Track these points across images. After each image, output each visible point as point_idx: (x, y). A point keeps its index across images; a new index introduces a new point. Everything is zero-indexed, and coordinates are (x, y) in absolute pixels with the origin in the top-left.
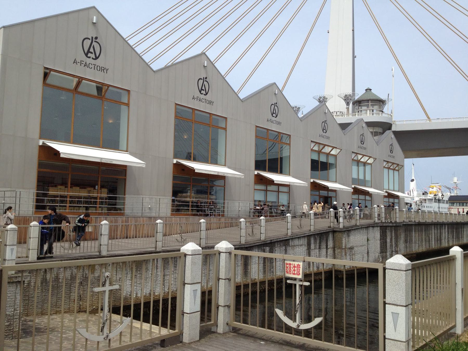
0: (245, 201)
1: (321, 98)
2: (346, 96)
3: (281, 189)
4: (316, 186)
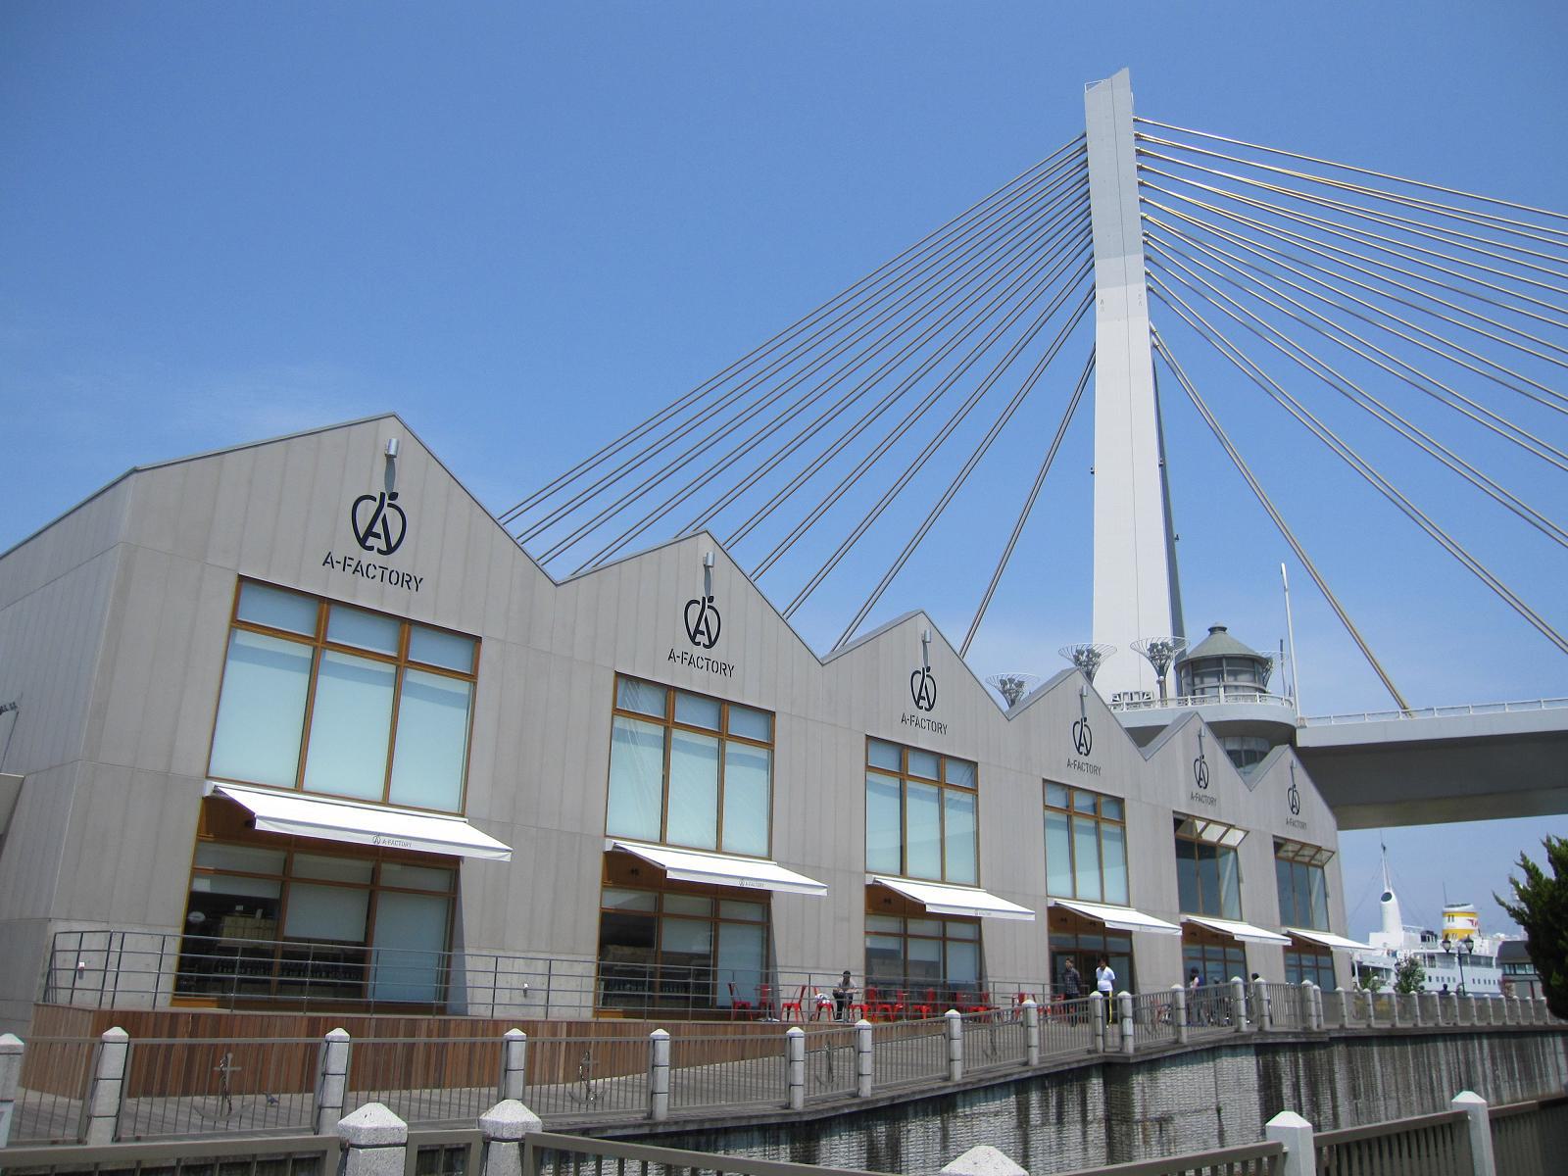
0: (834, 970)
1: (1082, 655)
2: (1153, 646)
3: (953, 930)
4: (1066, 920)
